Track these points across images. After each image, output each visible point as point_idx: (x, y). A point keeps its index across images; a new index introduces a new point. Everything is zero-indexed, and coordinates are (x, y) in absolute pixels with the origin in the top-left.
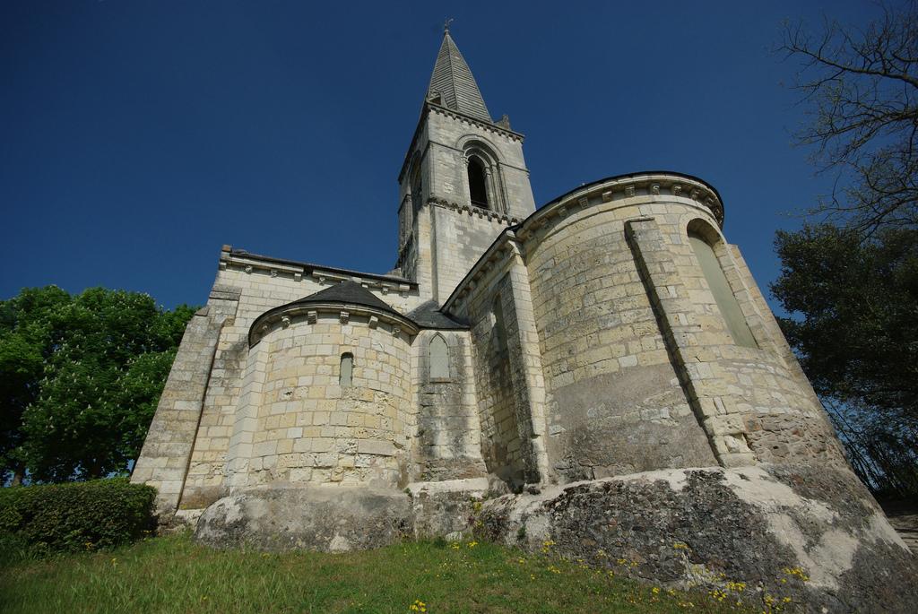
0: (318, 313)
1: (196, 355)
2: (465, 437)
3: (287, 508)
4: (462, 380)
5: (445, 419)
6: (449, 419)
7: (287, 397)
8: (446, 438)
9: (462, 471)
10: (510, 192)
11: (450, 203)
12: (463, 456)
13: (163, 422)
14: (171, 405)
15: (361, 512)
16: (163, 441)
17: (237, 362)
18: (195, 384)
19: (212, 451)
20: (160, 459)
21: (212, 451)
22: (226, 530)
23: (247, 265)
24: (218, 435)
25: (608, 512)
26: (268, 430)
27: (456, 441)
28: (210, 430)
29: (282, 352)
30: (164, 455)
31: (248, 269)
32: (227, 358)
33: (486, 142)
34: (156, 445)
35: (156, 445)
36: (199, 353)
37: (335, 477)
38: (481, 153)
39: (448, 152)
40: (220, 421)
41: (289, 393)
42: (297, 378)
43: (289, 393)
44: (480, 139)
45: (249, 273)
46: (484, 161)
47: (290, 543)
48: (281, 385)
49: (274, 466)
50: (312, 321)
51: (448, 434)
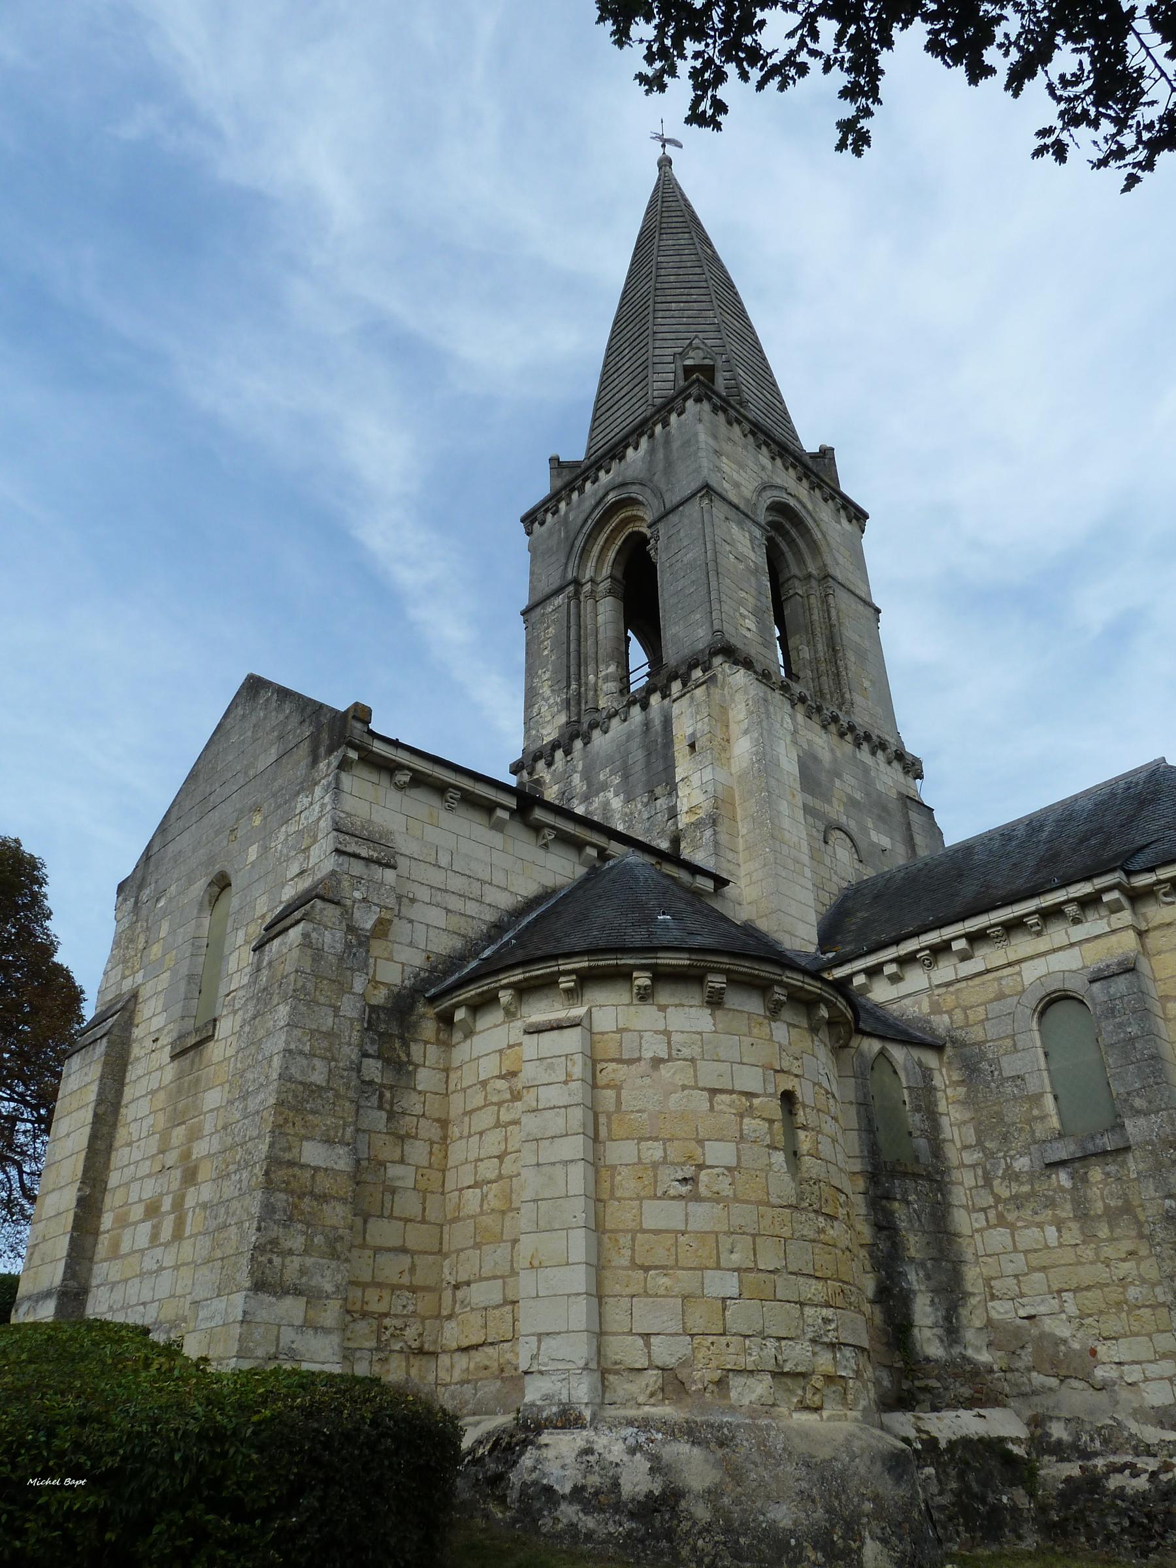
0: (730, 982)
1: (330, 1012)
2: (961, 1310)
3: (761, 1469)
4: (942, 1173)
5: (922, 1264)
6: (929, 1264)
7: (684, 1189)
8: (929, 1309)
9: (966, 1391)
10: (851, 657)
11: (759, 668)
12: (964, 1357)
13: (282, 1196)
14: (295, 1151)
15: (887, 1488)
16: (290, 1252)
17: (406, 1044)
18: (337, 1096)
19: (379, 1285)
20: (289, 1301)
21: (379, 1285)
22: (632, 1516)
23: (401, 767)
24: (390, 1244)
25: (120, 1366)
26: (646, 1269)
27: (948, 1318)
28: (370, 1226)
29: (643, 1067)
30: (297, 1292)
31: (403, 777)
32: (382, 1028)
33: (803, 513)
34: (277, 1260)
35: (277, 1260)
36: (336, 1009)
37: (813, 1399)
38: (792, 543)
39: (740, 524)
40: (388, 1205)
41: (685, 1180)
42: (700, 1142)
43: (685, 1180)
44: (792, 502)
45: (401, 788)
46: (789, 556)
47: (791, 1554)
48: (658, 1154)
49: (686, 1363)
50: (715, 1001)
51: (932, 1301)
